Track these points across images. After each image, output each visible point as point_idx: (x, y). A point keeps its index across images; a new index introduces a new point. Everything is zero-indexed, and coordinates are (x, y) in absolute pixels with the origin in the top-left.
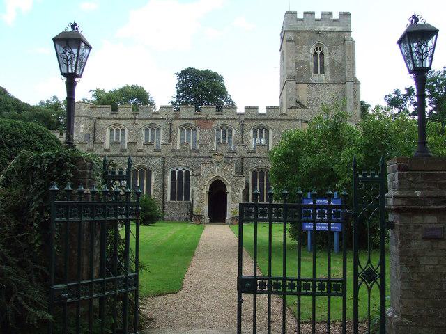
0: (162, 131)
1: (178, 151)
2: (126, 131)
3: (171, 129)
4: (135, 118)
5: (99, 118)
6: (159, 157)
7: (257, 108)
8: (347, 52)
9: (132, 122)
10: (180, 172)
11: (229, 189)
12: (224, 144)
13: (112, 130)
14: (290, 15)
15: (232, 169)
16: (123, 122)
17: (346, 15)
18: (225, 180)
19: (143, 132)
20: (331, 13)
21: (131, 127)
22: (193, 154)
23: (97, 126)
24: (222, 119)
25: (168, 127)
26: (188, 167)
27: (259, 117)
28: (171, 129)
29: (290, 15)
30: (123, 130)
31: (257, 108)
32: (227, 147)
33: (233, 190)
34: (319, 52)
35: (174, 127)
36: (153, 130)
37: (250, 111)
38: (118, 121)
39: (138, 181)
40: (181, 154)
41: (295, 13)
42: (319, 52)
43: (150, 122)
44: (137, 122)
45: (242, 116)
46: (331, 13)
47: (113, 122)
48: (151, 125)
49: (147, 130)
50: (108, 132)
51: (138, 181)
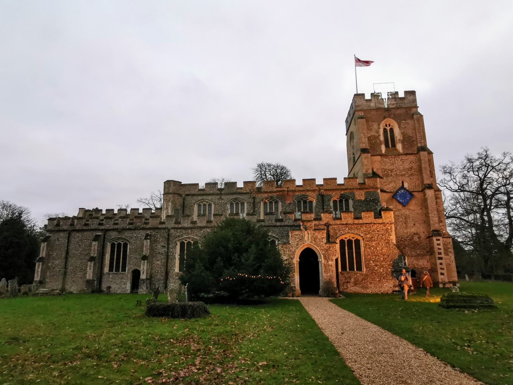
0: (246, 204)
1: (263, 221)
2: (213, 206)
3: (254, 202)
4: (221, 194)
5: (188, 195)
6: (164, 229)
7: (335, 179)
8: (417, 125)
9: (218, 197)
10: (350, 241)
11: (322, 260)
12: (271, 213)
13: (199, 206)
14: (359, 96)
15: (322, 235)
16: (210, 197)
17: (411, 93)
18: (317, 249)
19: (229, 206)
20: (397, 93)
21: (217, 201)
22: (278, 224)
23: (186, 202)
24: (304, 191)
25: (251, 201)
26: (274, 237)
27: (338, 187)
28: (254, 202)
29: (359, 96)
30: (210, 205)
31: (335, 179)
32: (256, 217)
33: (325, 259)
34: (388, 128)
35: (257, 200)
36: (237, 204)
37: (306, 182)
38: (205, 197)
39: (346, 248)
40: (267, 224)
41: (363, 95)
42: (388, 128)
43: (235, 196)
44: (223, 197)
45: (321, 187)
46: (397, 93)
47: (200, 198)
48: (236, 199)
49: (232, 204)
50: (196, 208)
51: (346, 248)
